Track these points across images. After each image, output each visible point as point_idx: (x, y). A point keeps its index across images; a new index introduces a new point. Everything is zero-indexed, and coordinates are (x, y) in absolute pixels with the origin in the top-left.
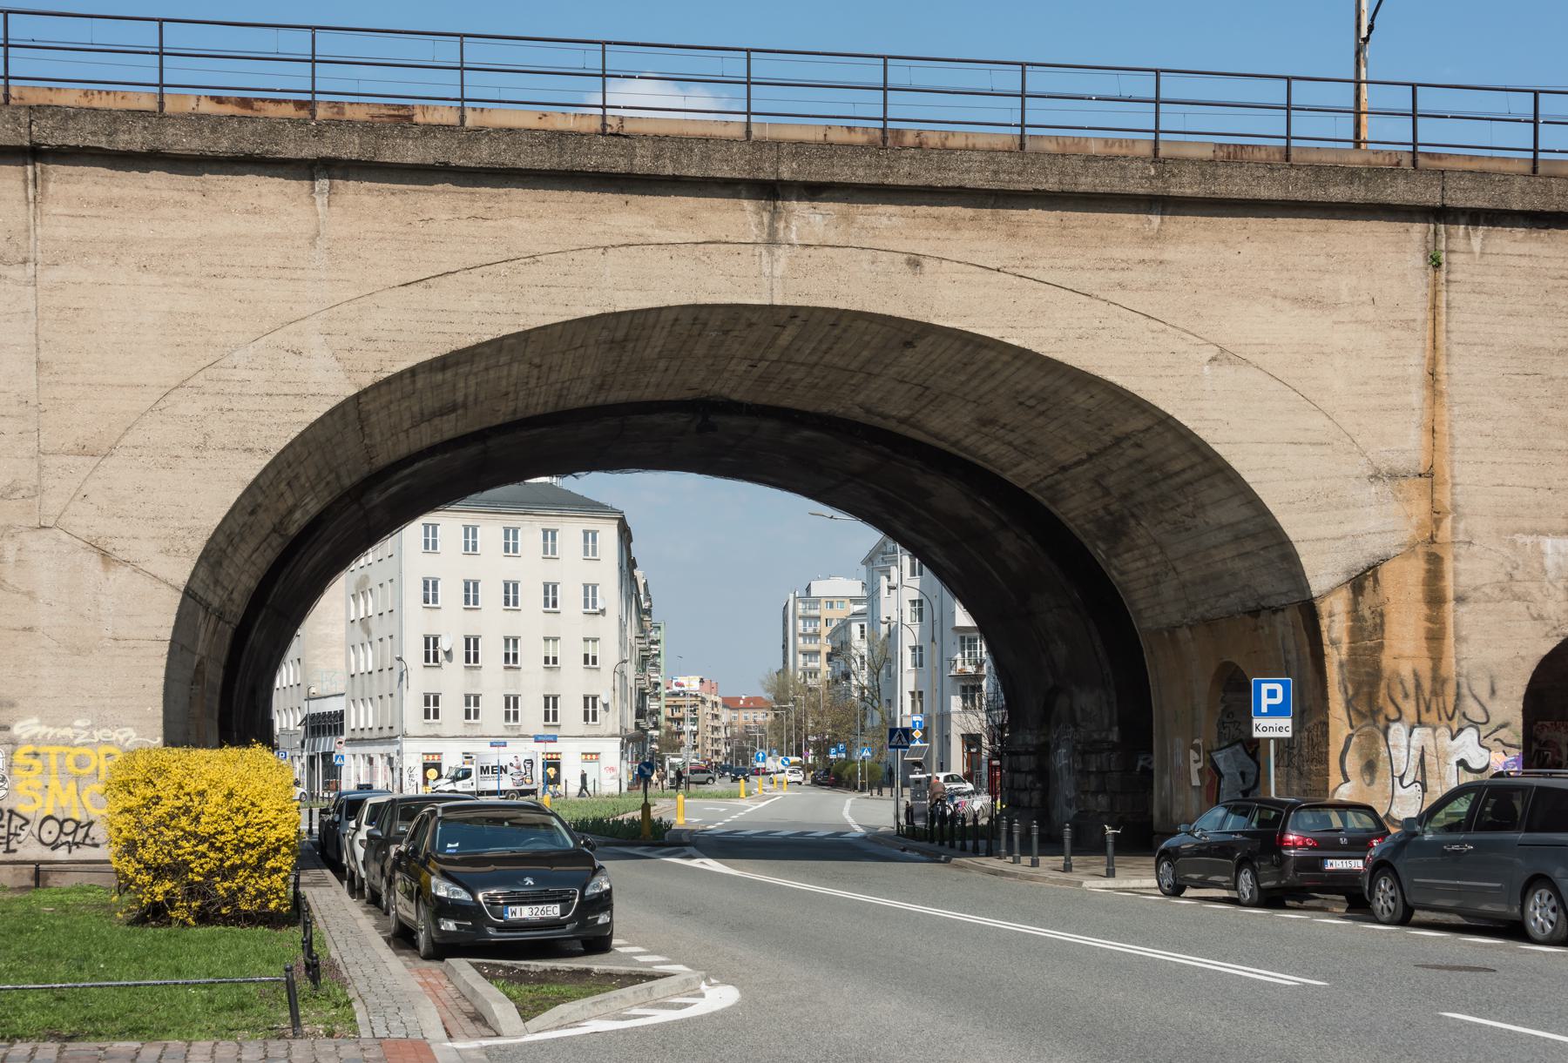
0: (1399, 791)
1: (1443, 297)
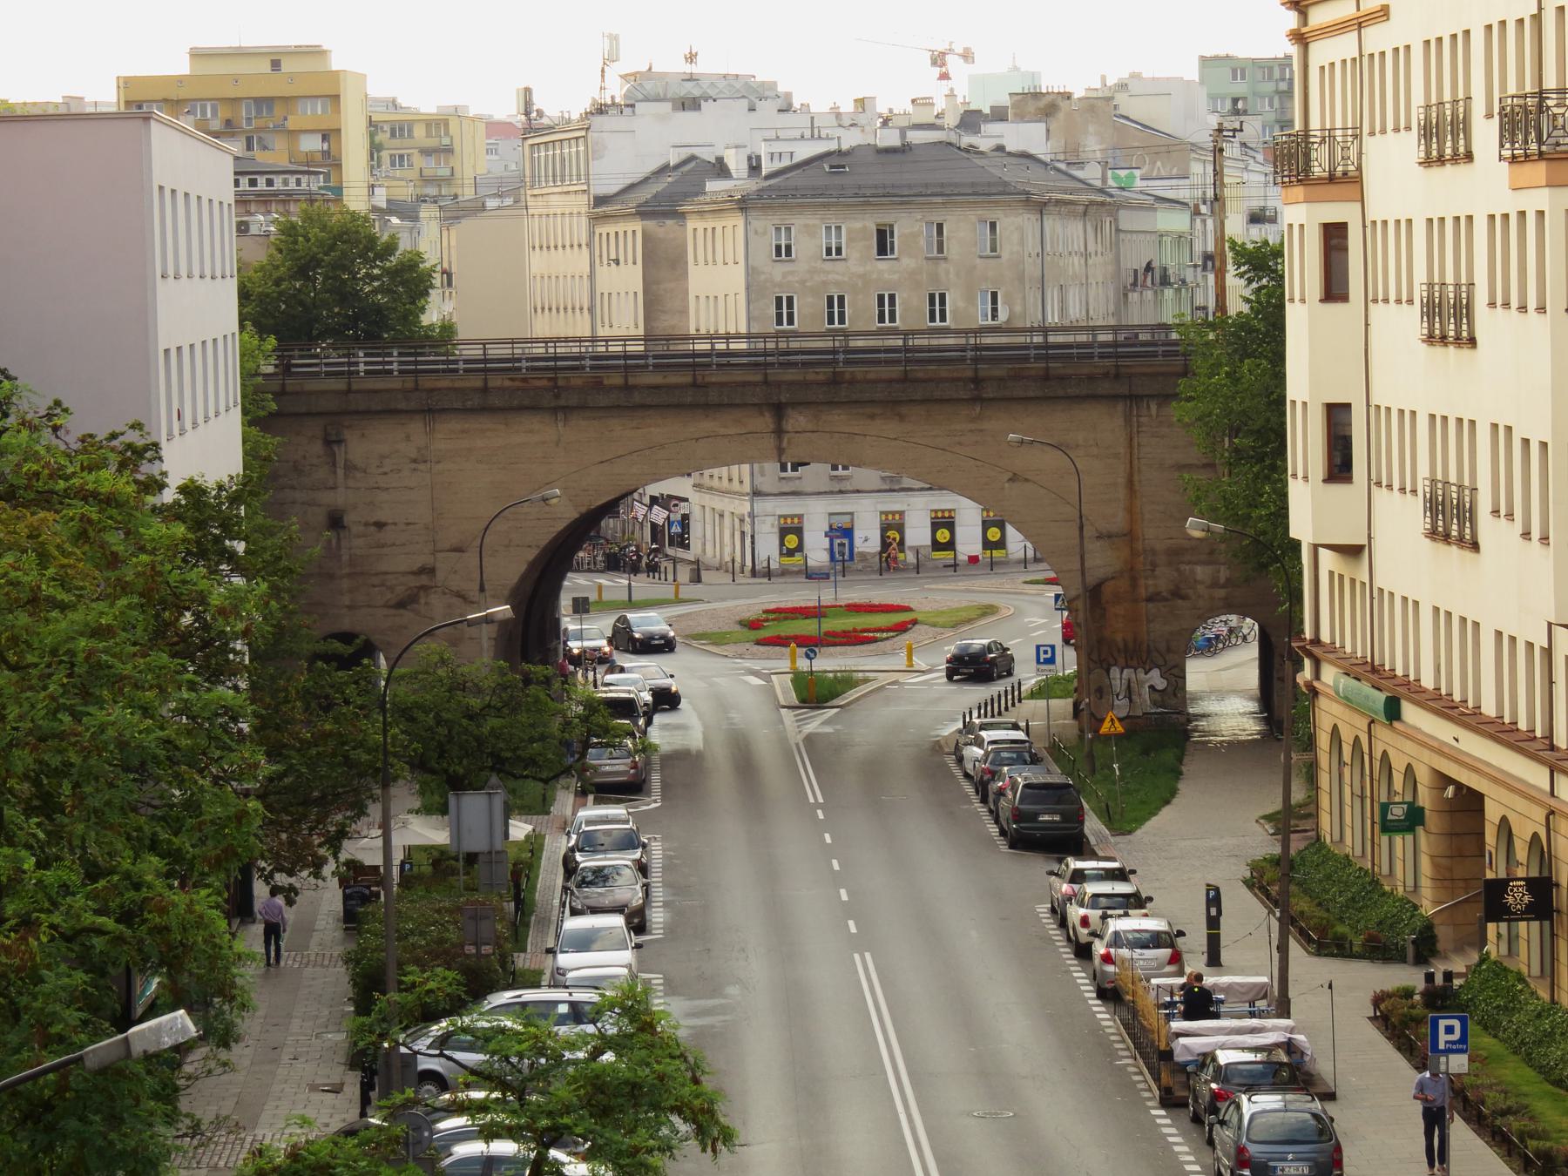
0: (1116, 702)
1: (1135, 440)
